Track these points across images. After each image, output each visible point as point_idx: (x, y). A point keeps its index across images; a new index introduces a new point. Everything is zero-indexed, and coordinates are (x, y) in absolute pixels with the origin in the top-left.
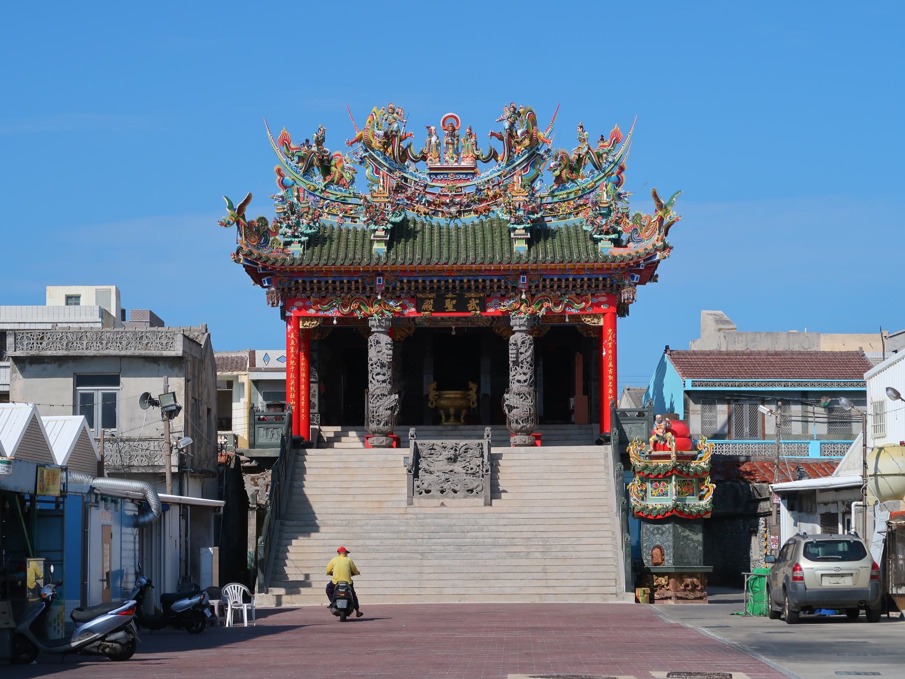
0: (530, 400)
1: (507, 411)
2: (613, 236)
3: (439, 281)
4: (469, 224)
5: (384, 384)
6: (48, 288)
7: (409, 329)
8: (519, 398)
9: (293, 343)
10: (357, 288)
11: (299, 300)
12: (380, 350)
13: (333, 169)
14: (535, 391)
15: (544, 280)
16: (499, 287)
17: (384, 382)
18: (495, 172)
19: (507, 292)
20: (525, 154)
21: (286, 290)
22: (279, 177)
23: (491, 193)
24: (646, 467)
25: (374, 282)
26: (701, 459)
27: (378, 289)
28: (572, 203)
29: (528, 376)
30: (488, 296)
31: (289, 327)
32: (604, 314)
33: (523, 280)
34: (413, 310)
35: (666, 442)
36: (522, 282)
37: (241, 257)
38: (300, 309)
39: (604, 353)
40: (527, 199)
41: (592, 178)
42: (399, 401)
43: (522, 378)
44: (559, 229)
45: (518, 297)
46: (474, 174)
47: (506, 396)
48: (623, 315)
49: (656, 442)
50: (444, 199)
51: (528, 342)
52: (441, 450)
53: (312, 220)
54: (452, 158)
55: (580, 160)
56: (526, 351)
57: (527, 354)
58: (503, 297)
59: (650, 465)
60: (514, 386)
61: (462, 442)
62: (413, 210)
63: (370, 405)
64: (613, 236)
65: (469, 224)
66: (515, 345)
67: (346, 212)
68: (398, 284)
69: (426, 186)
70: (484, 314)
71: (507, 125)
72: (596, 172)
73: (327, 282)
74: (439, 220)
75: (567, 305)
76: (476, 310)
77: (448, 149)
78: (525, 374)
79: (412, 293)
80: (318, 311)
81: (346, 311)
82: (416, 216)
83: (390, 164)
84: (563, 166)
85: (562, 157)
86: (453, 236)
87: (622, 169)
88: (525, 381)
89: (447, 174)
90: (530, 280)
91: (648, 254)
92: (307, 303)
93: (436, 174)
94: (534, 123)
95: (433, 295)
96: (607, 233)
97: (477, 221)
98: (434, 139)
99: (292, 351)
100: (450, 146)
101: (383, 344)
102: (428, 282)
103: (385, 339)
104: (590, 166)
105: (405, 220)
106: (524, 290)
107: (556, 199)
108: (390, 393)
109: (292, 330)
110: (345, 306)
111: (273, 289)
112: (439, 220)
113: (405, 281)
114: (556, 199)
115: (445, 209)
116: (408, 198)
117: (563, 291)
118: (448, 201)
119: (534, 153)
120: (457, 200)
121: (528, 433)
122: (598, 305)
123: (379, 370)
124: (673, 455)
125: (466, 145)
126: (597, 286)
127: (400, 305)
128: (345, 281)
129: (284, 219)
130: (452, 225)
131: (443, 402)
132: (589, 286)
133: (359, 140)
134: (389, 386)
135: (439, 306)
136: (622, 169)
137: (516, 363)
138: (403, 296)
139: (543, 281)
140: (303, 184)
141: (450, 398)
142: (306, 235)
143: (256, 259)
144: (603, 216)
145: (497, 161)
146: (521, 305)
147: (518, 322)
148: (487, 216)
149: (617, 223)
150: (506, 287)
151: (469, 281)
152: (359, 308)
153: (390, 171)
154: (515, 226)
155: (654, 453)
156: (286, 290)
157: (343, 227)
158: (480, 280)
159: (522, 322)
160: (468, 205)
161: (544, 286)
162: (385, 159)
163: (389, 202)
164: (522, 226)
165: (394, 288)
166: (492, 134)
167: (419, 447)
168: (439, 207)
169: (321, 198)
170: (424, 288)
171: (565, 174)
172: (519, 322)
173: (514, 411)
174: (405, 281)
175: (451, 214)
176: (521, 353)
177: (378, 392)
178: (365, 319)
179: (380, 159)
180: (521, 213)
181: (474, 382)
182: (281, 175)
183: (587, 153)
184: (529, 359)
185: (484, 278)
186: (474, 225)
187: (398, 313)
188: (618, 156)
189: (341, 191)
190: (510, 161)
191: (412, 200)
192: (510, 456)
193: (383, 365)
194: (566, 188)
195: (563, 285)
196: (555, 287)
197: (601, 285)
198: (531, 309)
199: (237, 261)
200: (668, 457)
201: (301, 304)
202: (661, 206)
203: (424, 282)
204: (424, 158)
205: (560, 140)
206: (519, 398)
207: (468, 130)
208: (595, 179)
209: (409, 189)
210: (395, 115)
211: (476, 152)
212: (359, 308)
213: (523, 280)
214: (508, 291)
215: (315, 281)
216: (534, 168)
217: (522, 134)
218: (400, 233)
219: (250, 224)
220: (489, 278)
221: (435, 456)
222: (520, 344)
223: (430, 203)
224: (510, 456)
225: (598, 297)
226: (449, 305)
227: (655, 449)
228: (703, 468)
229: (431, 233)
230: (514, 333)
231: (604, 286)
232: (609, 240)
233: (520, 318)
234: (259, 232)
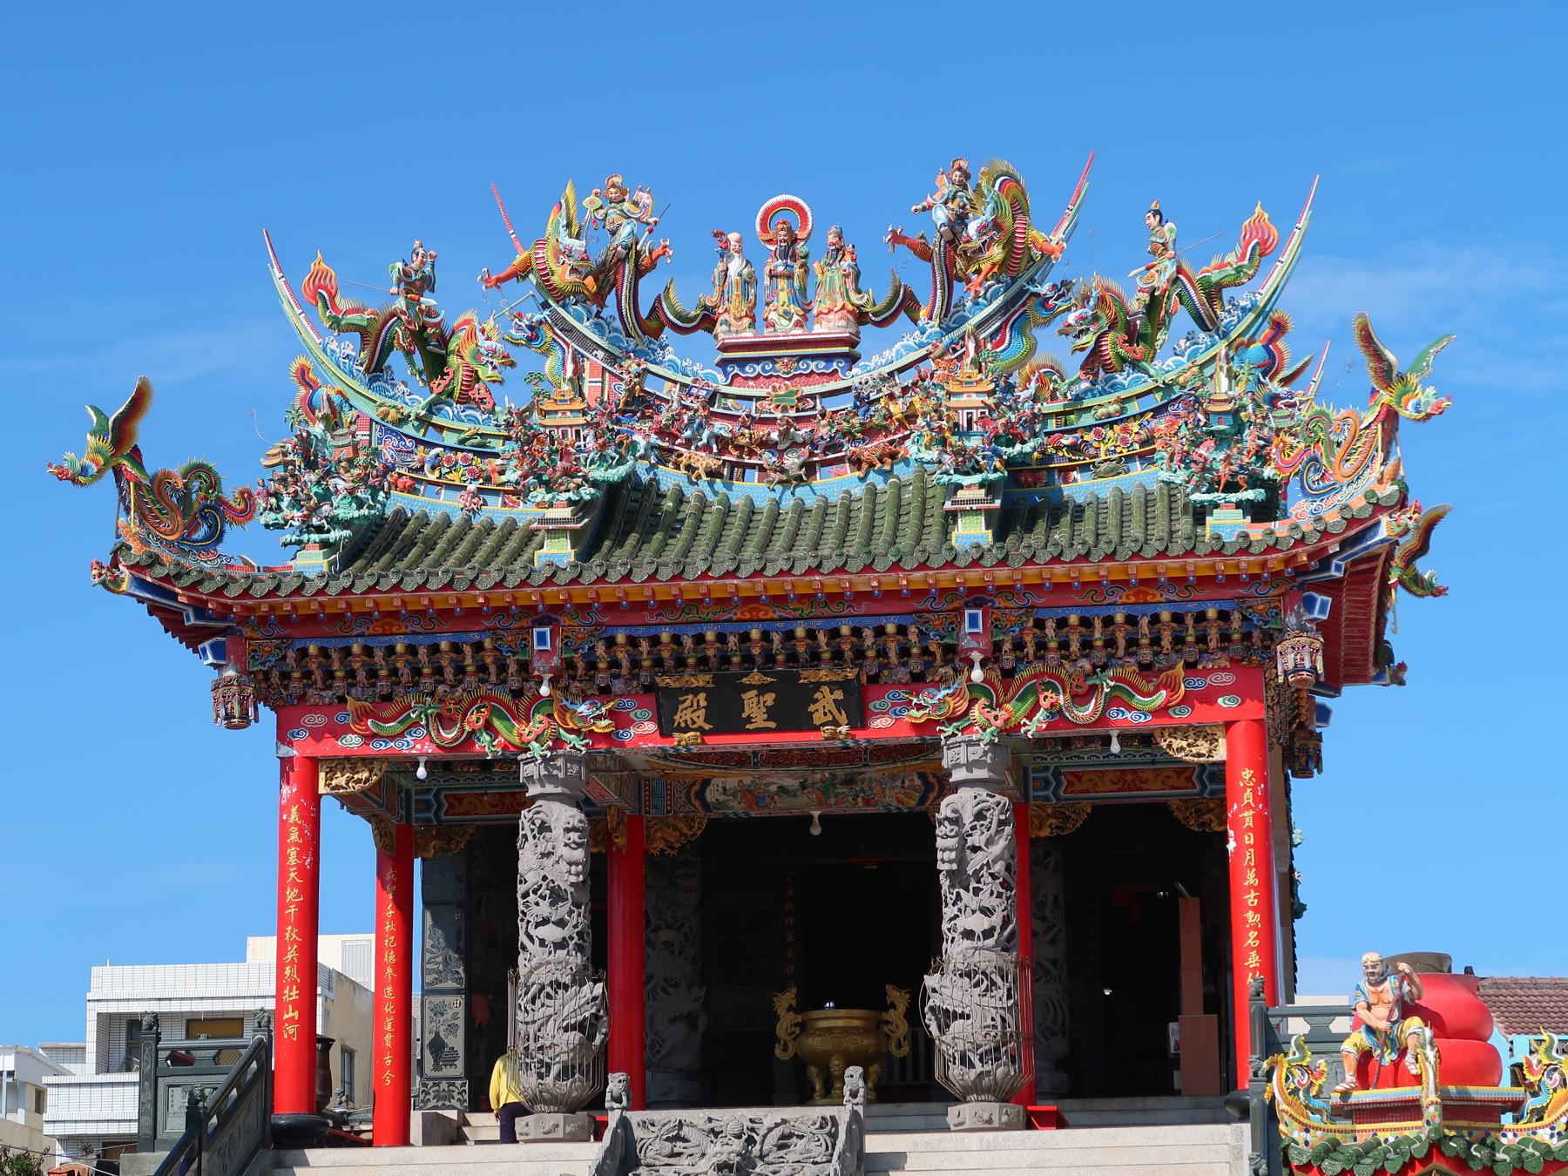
0: (1003, 992)
1: (934, 1029)
2: (1250, 494)
3: (721, 638)
4: (835, 498)
5: (561, 953)
6: (250, 940)
7: (689, 821)
8: (970, 992)
9: (294, 836)
10: (482, 668)
11: (316, 708)
12: (551, 849)
13: (453, 360)
14: (1020, 965)
15: (1040, 624)
16: (904, 652)
17: (561, 945)
18: (909, 349)
19: (929, 665)
20: (995, 296)
21: (275, 679)
22: (303, 391)
23: (897, 409)
24: (1332, 1148)
25: (526, 646)
26: (1539, 1114)
27: (538, 666)
28: (1134, 426)
29: (996, 920)
30: (874, 679)
31: (286, 790)
32: (1228, 725)
33: (973, 623)
34: (650, 727)
35: (1403, 1053)
36: (971, 631)
37: (126, 574)
38: (317, 734)
39: (1231, 846)
40: (991, 401)
41: (1195, 353)
42: (606, 1002)
43: (978, 923)
44: (1098, 504)
45: (964, 677)
46: (852, 359)
47: (930, 981)
48: (1304, 773)
49: (1366, 1056)
50: (760, 432)
51: (994, 816)
52: (705, 1141)
53: (363, 479)
54: (787, 315)
55: (1154, 305)
56: (989, 842)
57: (993, 850)
58: (918, 681)
59: (1346, 1141)
60: (956, 951)
61: (769, 1116)
62: (677, 467)
63: (521, 1016)
64: (1250, 494)
65: (835, 498)
66: (956, 821)
67: (488, 480)
68: (601, 650)
69: (713, 397)
70: (861, 736)
71: (941, 215)
72: (1202, 336)
73: (390, 650)
74: (752, 490)
75: (1112, 700)
76: (836, 723)
77: (774, 291)
78: (987, 912)
79: (645, 677)
80: (370, 737)
81: (449, 735)
82: (684, 484)
83: (612, 341)
84: (1104, 322)
85: (1101, 299)
86: (770, 515)
87: (1279, 328)
88: (988, 934)
89: (772, 359)
90: (994, 625)
91: (1352, 522)
92: (339, 718)
93: (742, 363)
94: (1019, 207)
95: (702, 680)
96: (1232, 487)
97: (858, 491)
98: (735, 266)
99: (293, 859)
100: (782, 283)
101: (557, 832)
102: (688, 642)
103: (563, 816)
104: (1182, 320)
105: (632, 476)
106: (977, 656)
107: (1087, 419)
108: (578, 980)
109: (294, 799)
110: (445, 720)
111: (230, 673)
112: (752, 490)
113: (621, 638)
114: (1087, 419)
115: (767, 458)
116: (661, 433)
117: (1099, 656)
118: (775, 436)
119: (1022, 292)
120: (803, 432)
121: (1003, 1094)
122: (1209, 697)
123: (544, 909)
124: (1428, 1095)
125: (830, 281)
126: (1202, 639)
127: (611, 714)
128: (444, 645)
129: (283, 480)
130: (788, 503)
131: (814, 1043)
132: (1178, 640)
133: (522, 273)
134: (577, 960)
135: (726, 716)
136: (1279, 328)
137: (959, 877)
138: (618, 686)
139: (1037, 628)
140: (366, 404)
141: (829, 1030)
142: (346, 524)
143: (167, 579)
144: (1221, 439)
145: (915, 321)
146: (972, 702)
147: (962, 755)
148: (887, 474)
149: (1263, 459)
150: (926, 651)
151: (811, 634)
152: (488, 727)
153: (612, 358)
154: (957, 478)
155: (1361, 1097)
156: (275, 679)
157: (477, 522)
158: (845, 630)
159: (976, 753)
160: (833, 446)
161: (1041, 646)
162: (598, 328)
163: (588, 424)
164: (977, 478)
165: (592, 666)
166: (897, 238)
167: (638, 1133)
168: (751, 453)
169: (419, 442)
170: (680, 662)
171: (1113, 345)
172: (964, 755)
173: (957, 1026)
174: (621, 638)
175: (783, 471)
176: (975, 849)
177: (543, 977)
178: (509, 761)
179: (585, 328)
180: (973, 443)
181: (900, 986)
182: (310, 385)
183: (1175, 281)
184: (999, 867)
185: (856, 622)
186: (849, 500)
187: (606, 736)
188: (1267, 291)
189: (475, 420)
190: (951, 316)
191: (674, 437)
192: (932, 1161)
193: (556, 896)
194: (1114, 387)
195: (1098, 635)
196: (1075, 647)
197: (1213, 634)
198: (1002, 714)
199: (112, 585)
200: (1410, 1110)
201: (319, 720)
202: (1386, 375)
203: (676, 639)
204: (707, 320)
205: (1100, 253)
206: (970, 992)
207: (832, 239)
208: (1201, 359)
209: (664, 407)
210: (626, 206)
211: (855, 298)
212: (488, 727)
213: (973, 623)
214: (934, 662)
215: (356, 649)
216: (1021, 333)
217: (982, 230)
218: (619, 514)
219: (160, 483)
220: (870, 621)
221: (684, 1161)
222: (972, 825)
223: (723, 443)
224: (932, 1161)
225: (1206, 673)
226: (755, 707)
227: (1364, 1080)
228: (1548, 1150)
229: (723, 524)
230: (955, 788)
231: (1225, 637)
232: (1238, 505)
233: (970, 743)
234: (198, 507)
